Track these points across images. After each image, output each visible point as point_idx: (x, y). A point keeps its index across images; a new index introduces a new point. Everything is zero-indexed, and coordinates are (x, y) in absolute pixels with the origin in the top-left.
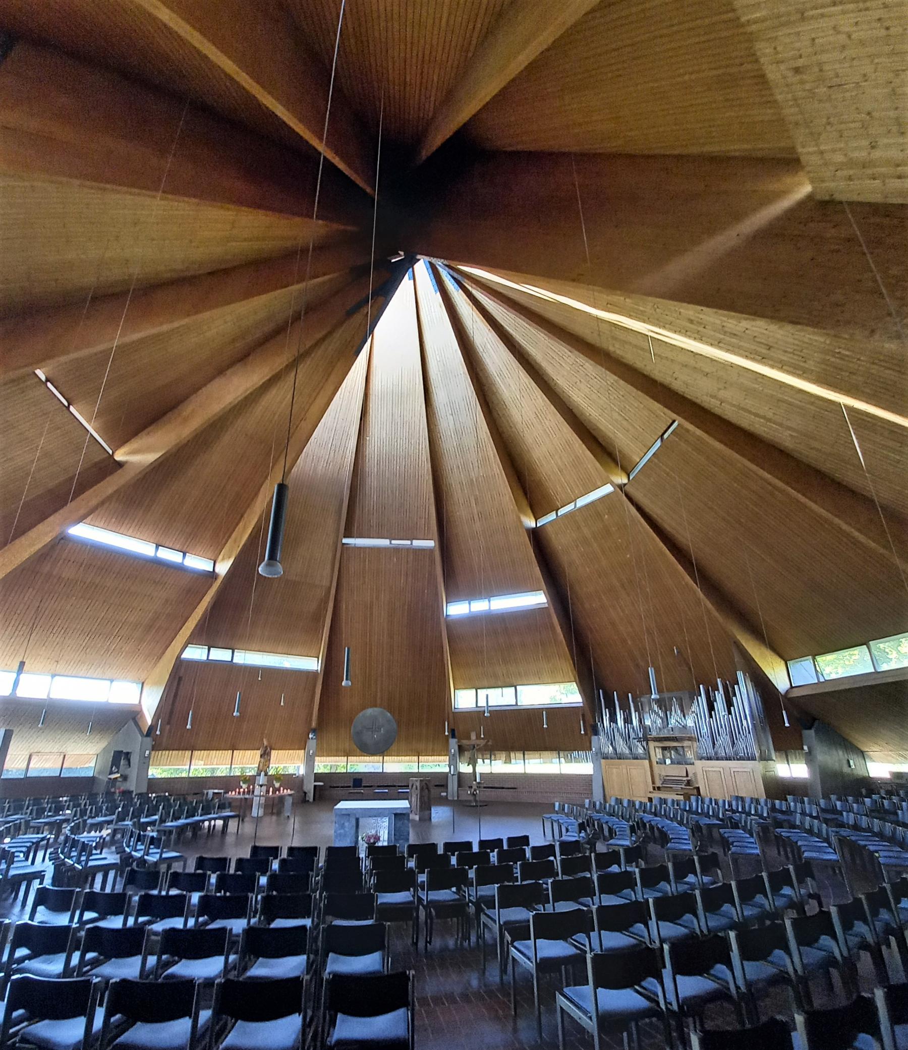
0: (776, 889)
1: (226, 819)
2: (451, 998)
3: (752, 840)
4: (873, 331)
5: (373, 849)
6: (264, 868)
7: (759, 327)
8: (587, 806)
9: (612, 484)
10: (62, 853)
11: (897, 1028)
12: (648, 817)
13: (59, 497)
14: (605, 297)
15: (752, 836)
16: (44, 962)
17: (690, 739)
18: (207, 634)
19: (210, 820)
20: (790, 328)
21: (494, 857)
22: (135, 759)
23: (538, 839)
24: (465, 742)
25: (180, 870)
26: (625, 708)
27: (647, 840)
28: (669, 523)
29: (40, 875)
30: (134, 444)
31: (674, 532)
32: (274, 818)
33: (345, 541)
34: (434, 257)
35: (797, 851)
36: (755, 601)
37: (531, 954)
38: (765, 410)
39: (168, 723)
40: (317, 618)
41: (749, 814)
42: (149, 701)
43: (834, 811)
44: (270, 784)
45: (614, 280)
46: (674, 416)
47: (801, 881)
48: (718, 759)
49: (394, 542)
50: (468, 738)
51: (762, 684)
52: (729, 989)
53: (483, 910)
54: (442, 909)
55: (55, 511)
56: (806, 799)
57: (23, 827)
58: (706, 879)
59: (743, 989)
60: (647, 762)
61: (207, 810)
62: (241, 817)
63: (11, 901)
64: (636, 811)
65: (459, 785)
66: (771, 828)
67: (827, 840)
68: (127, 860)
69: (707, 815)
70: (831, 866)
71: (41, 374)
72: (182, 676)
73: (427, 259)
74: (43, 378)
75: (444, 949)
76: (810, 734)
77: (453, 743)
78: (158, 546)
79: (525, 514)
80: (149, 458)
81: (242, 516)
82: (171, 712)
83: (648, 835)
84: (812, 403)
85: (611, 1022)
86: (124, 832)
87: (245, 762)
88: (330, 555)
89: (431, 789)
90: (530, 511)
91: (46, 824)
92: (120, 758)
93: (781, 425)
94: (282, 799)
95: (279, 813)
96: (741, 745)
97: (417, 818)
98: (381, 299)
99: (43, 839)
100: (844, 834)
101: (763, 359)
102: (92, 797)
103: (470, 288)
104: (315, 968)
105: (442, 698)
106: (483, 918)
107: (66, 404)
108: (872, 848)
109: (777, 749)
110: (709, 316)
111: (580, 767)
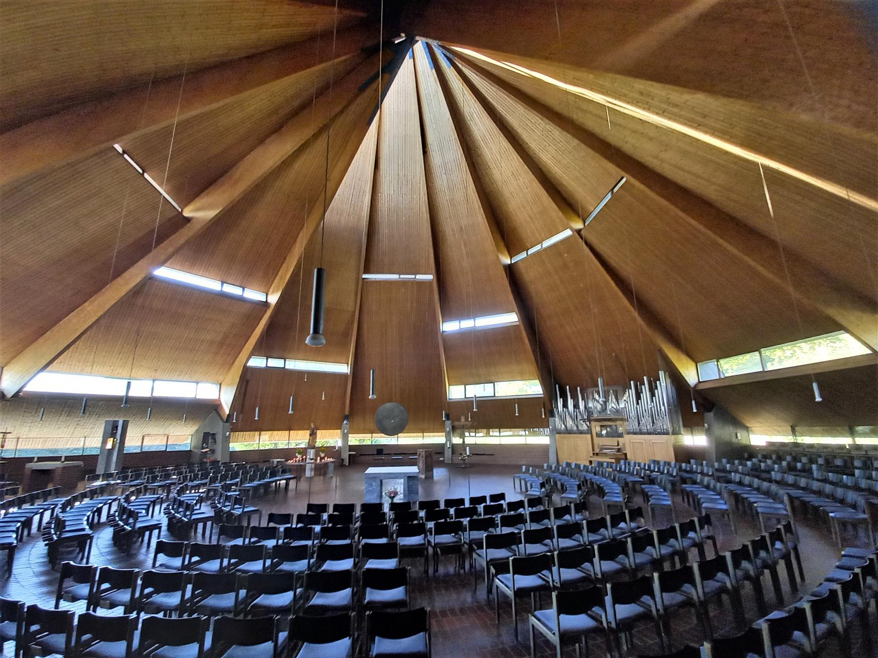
0: (684, 534)
1: (288, 480)
2: (453, 612)
3: (666, 494)
4: (791, 105)
5: (393, 506)
6: (317, 520)
7: (698, 99)
8: (545, 468)
9: (572, 229)
10: (173, 509)
11: (777, 649)
12: (589, 476)
13: (144, 247)
14: (571, 73)
15: (665, 490)
16: (165, 596)
17: (622, 420)
18: (264, 347)
19: (276, 481)
20: (724, 100)
21: (481, 508)
22: (219, 438)
23: (512, 497)
24: (457, 423)
25: (257, 525)
26: (575, 397)
27: (588, 494)
28: (614, 261)
29: (158, 526)
30: (197, 203)
31: (617, 267)
32: (322, 478)
33: (364, 276)
34: (430, 38)
35: (697, 504)
36: (677, 318)
37: (511, 585)
38: (697, 168)
39: (242, 412)
40: (346, 335)
41: (662, 473)
42: (226, 398)
43: (724, 470)
44: (317, 455)
45: (580, 59)
46: (623, 173)
47: (702, 527)
48: (641, 434)
49: (402, 276)
50: (459, 420)
51: (677, 380)
52: (651, 611)
53: (474, 550)
54: (447, 549)
55: (142, 257)
56: (704, 462)
57: (143, 490)
58: (633, 525)
59: (662, 611)
60: (589, 436)
61: (273, 474)
62: (297, 478)
63: (139, 544)
64: (581, 471)
65: (453, 453)
66: (678, 484)
67: (720, 494)
68: (219, 513)
69: (632, 474)
70: (723, 513)
71: (118, 148)
72: (248, 378)
73: (425, 40)
74: (120, 150)
75: (447, 575)
76: (710, 415)
77: (448, 423)
78: (223, 283)
79: (502, 253)
80: (210, 214)
81: (285, 259)
82: (243, 406)
83: (591, 489)
84: (735, 163)
85: (568, 638)
86: (215, 490)
87: (298, 439)
88: (353, 288)
89: (432, 457)
90: (506, 253)
91: (160, 486)
92: (208, 437)
93: (708, 181)
94: (326, 464)
95: (325, 474)
96: (659, 424)
97: (423, 477)
98: (386, 76)
99: (158, 498)
100: (732, 488)
101: (698, 126)
102: (190, 466)
103: (460, 66)
104: (358, 596)
105: (441, 392)
106: (474, 555)
107: (141, 171)
108: (752, 500)
109: (685, 426)
110: (658, 90)
111: (542, 439)
